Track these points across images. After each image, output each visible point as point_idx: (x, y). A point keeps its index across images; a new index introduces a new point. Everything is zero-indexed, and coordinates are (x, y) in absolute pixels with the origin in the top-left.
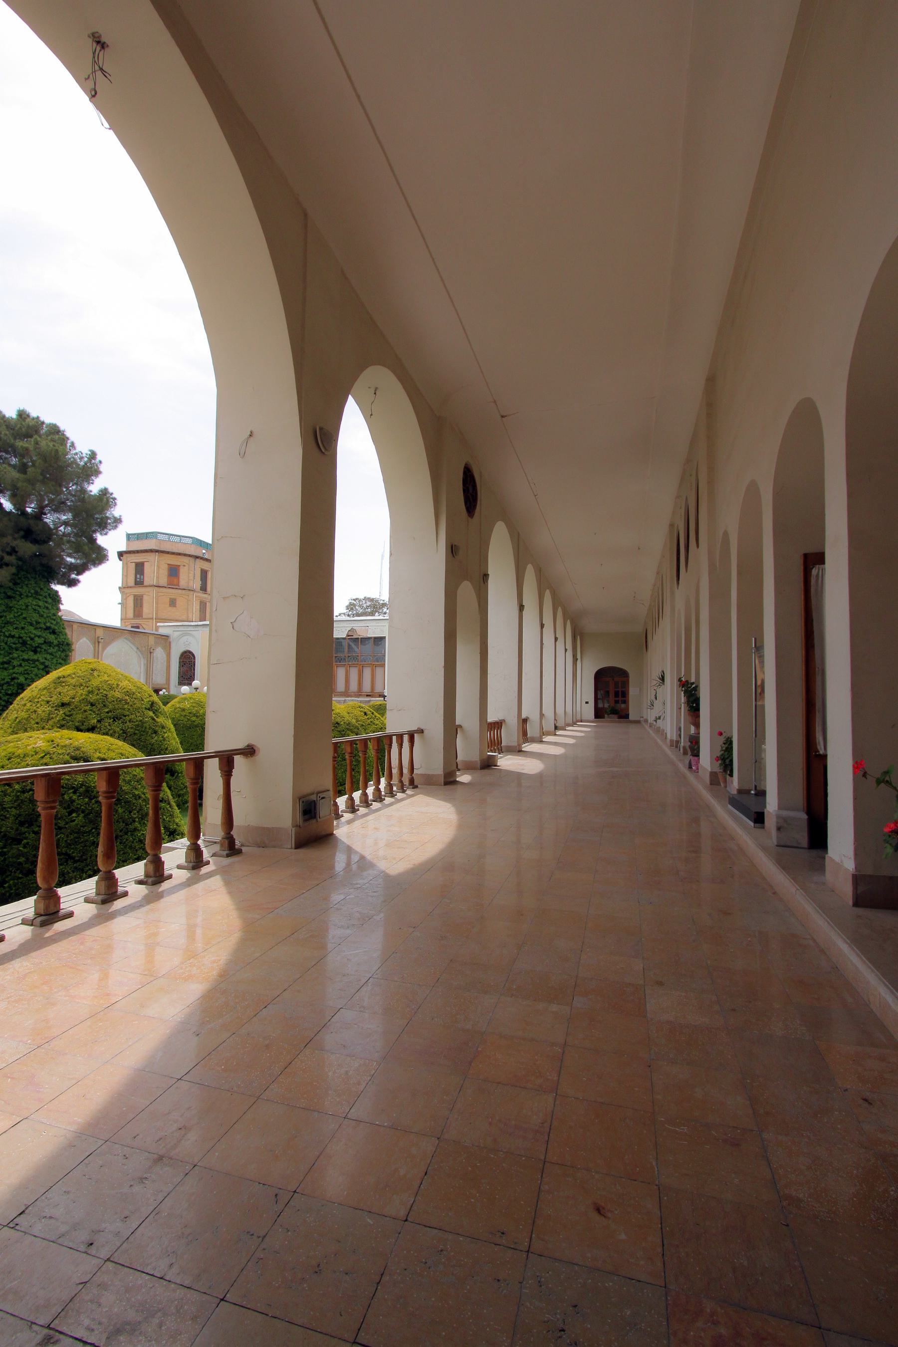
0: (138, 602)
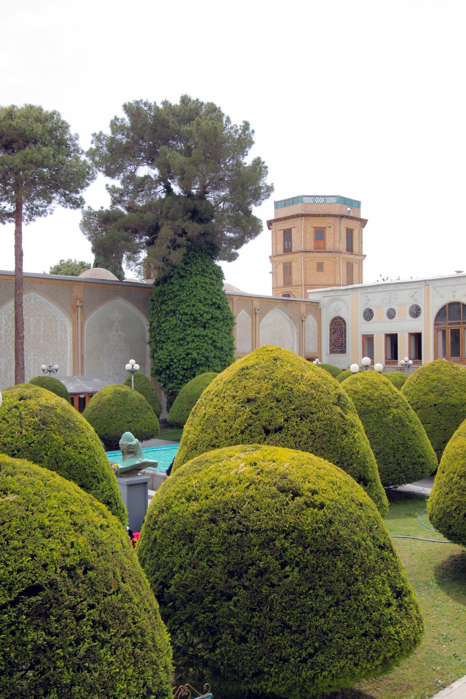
0: (288, 269)
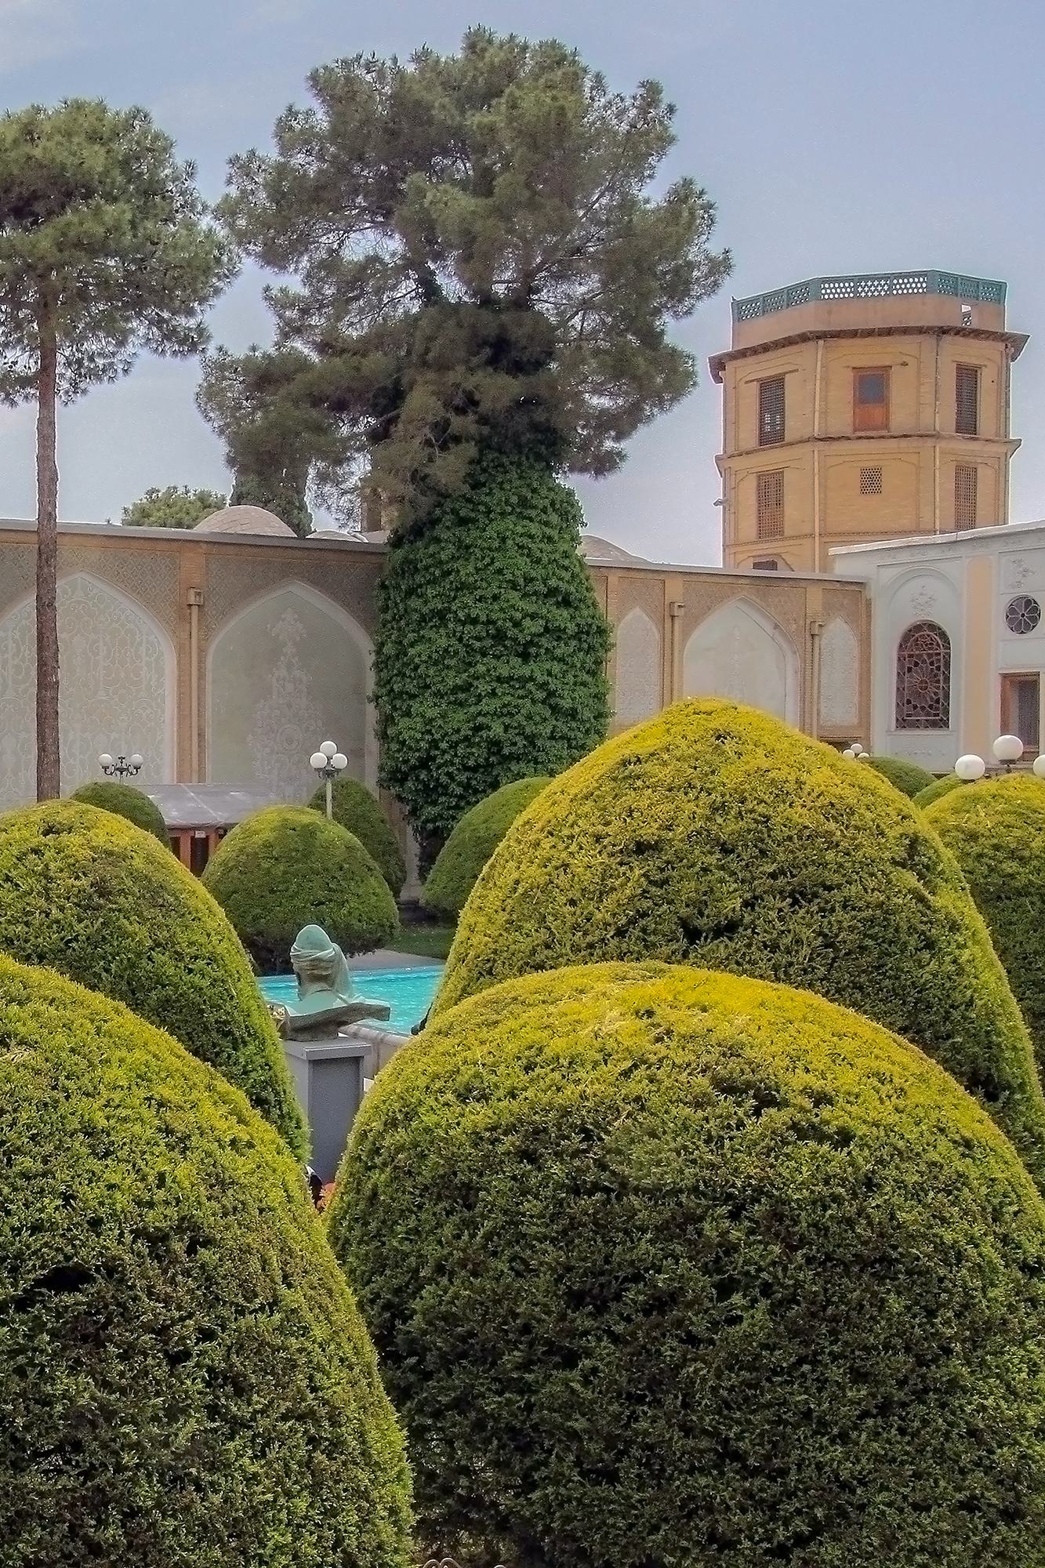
0: (770, 490)
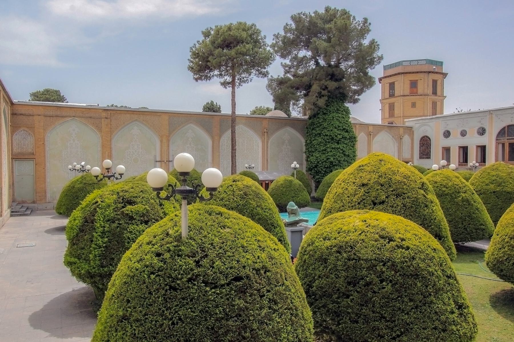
0: (392, 107)
